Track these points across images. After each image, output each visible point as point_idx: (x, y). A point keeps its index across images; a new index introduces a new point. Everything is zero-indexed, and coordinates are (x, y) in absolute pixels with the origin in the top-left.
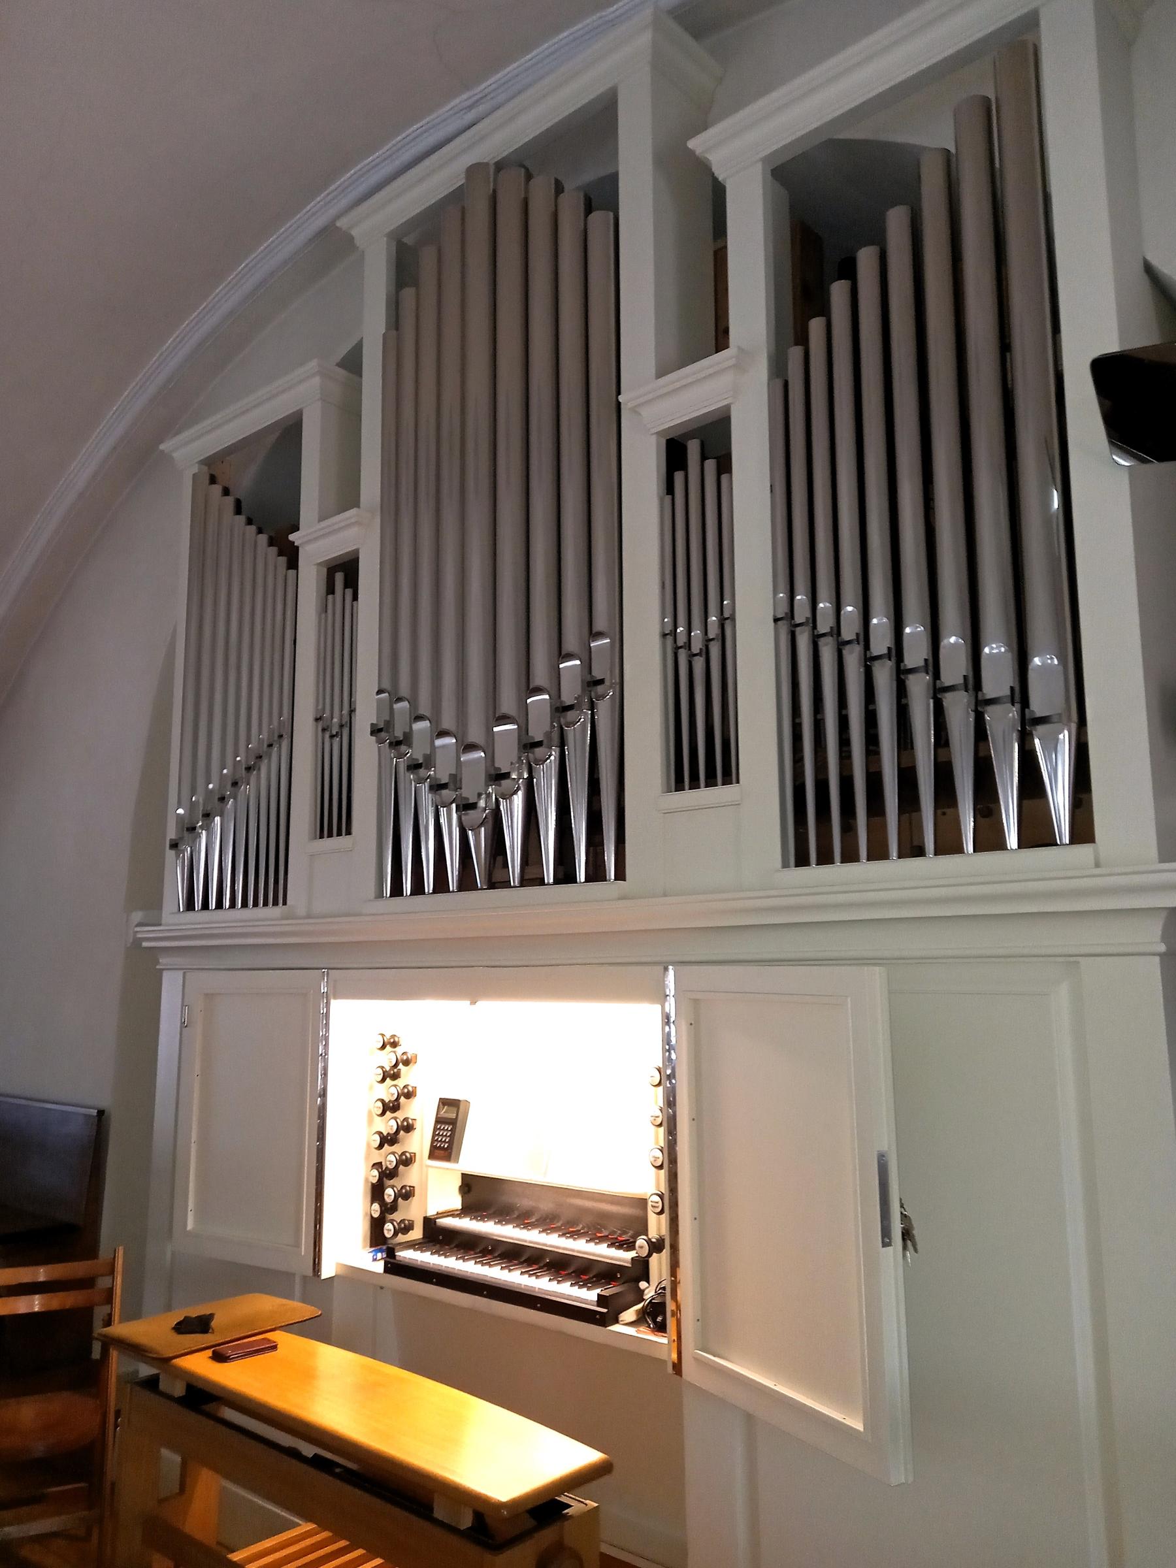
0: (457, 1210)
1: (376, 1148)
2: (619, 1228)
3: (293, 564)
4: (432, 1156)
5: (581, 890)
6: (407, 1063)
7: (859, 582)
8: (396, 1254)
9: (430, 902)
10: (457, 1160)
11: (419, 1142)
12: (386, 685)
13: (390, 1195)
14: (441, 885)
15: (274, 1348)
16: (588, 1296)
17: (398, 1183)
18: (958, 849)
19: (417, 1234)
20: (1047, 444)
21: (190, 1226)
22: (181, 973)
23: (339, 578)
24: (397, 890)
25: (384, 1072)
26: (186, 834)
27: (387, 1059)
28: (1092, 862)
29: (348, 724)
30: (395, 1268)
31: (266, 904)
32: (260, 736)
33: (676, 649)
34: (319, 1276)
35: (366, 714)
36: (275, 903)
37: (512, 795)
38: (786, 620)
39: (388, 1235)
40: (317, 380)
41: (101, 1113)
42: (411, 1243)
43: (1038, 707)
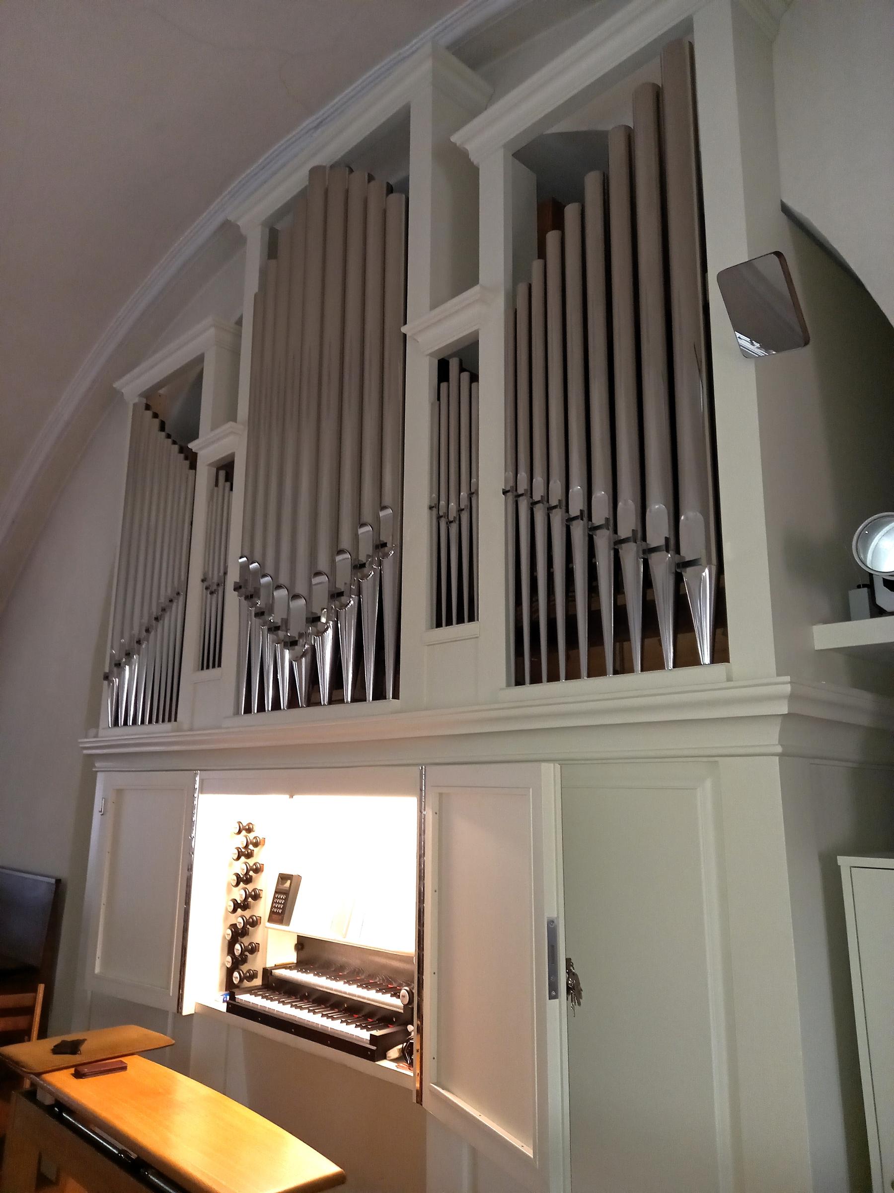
0: (293, 963)
1: (231, 913)
2: (405, 981)
3: (193, 466)
4: (270, 920)
5: (370, 706)
6: (256, 845)
7: (610, 473)
8: (236, 996)
9: (270, 715)
10: (288, 924)
11: (263, 908)
12: (246, 553)
13: (238, 950)
14: (276, 706)
15: (124, 1068)
16: (363, 1035)
17: (246, 941)
19: (258, 982)
20: (695, 349)
21: (97, 970)
23: (222, 474)
24: (248, 710)
25: (239, 852)
26: (115, 669)
27: (240, 841)
28: (724, 677)
29: (221, 583)
30: (234, 1008)
31: (163, 721)
32: (166, 592)
33: (439, 517)
34: (181, 1013)
35: (233, 576)
36: (170, 720)
37: (324, 632)
38: (511, 492)
39: (236, 981)
40: (212, 331)
41: (58, 881)
42: (249, 989)
43: (687, 553)
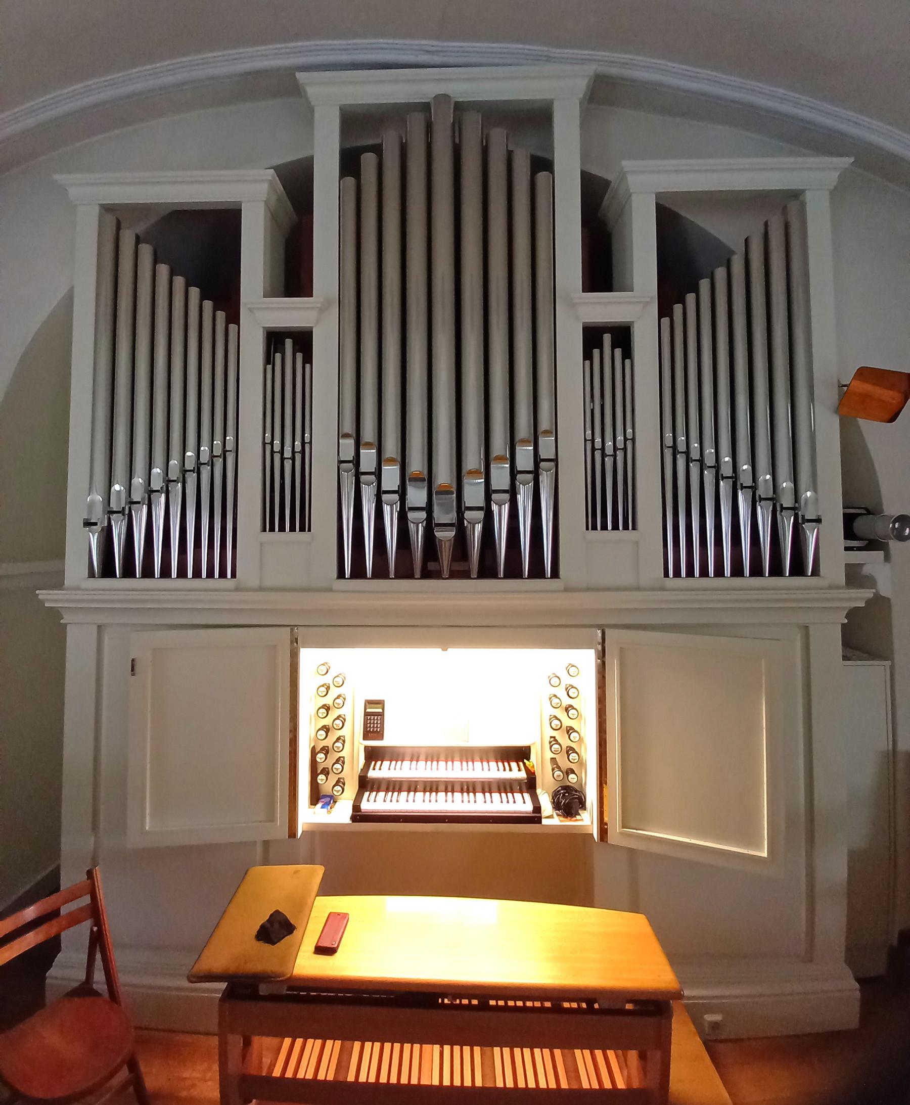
18: (133, 575)
22: (289, 629)
